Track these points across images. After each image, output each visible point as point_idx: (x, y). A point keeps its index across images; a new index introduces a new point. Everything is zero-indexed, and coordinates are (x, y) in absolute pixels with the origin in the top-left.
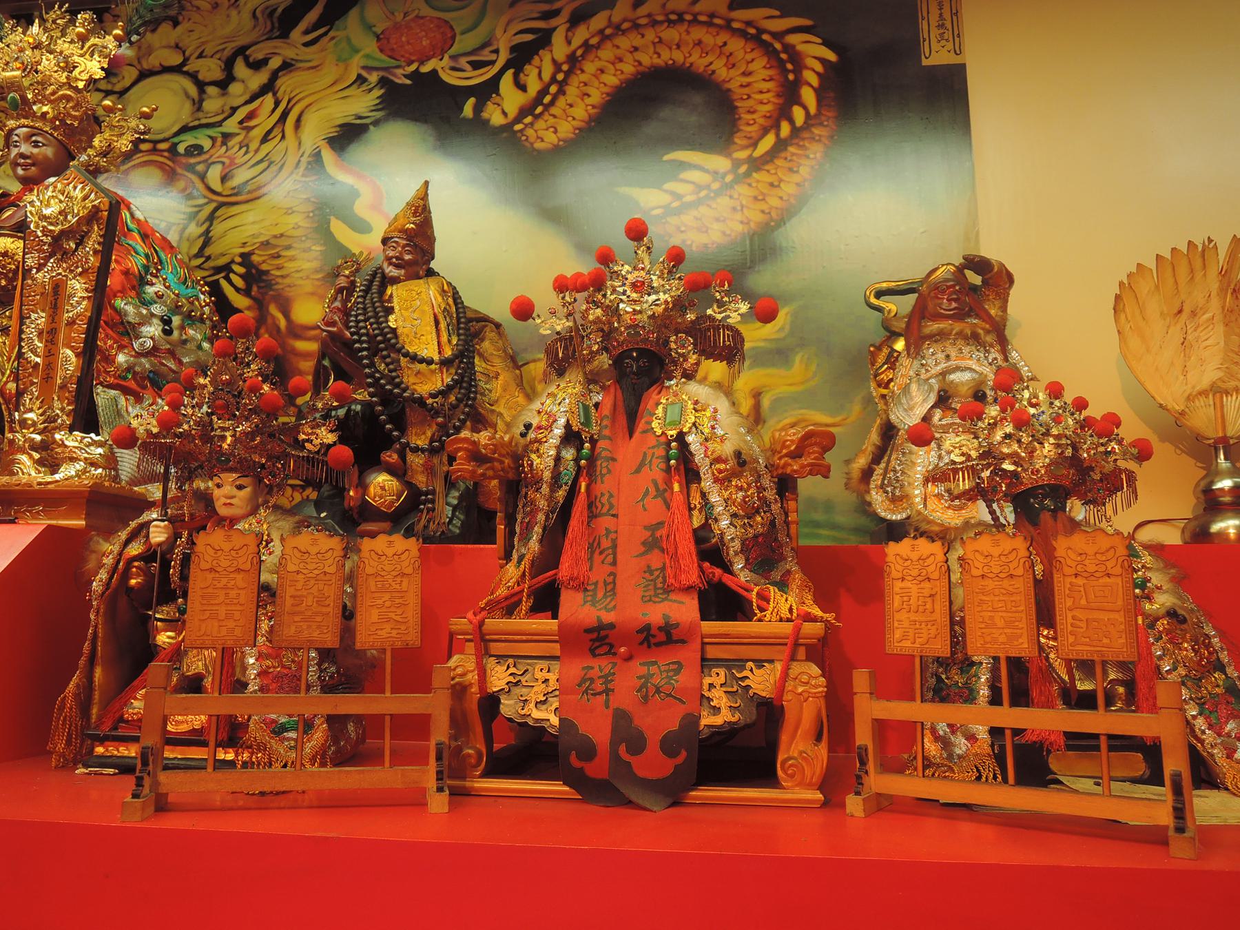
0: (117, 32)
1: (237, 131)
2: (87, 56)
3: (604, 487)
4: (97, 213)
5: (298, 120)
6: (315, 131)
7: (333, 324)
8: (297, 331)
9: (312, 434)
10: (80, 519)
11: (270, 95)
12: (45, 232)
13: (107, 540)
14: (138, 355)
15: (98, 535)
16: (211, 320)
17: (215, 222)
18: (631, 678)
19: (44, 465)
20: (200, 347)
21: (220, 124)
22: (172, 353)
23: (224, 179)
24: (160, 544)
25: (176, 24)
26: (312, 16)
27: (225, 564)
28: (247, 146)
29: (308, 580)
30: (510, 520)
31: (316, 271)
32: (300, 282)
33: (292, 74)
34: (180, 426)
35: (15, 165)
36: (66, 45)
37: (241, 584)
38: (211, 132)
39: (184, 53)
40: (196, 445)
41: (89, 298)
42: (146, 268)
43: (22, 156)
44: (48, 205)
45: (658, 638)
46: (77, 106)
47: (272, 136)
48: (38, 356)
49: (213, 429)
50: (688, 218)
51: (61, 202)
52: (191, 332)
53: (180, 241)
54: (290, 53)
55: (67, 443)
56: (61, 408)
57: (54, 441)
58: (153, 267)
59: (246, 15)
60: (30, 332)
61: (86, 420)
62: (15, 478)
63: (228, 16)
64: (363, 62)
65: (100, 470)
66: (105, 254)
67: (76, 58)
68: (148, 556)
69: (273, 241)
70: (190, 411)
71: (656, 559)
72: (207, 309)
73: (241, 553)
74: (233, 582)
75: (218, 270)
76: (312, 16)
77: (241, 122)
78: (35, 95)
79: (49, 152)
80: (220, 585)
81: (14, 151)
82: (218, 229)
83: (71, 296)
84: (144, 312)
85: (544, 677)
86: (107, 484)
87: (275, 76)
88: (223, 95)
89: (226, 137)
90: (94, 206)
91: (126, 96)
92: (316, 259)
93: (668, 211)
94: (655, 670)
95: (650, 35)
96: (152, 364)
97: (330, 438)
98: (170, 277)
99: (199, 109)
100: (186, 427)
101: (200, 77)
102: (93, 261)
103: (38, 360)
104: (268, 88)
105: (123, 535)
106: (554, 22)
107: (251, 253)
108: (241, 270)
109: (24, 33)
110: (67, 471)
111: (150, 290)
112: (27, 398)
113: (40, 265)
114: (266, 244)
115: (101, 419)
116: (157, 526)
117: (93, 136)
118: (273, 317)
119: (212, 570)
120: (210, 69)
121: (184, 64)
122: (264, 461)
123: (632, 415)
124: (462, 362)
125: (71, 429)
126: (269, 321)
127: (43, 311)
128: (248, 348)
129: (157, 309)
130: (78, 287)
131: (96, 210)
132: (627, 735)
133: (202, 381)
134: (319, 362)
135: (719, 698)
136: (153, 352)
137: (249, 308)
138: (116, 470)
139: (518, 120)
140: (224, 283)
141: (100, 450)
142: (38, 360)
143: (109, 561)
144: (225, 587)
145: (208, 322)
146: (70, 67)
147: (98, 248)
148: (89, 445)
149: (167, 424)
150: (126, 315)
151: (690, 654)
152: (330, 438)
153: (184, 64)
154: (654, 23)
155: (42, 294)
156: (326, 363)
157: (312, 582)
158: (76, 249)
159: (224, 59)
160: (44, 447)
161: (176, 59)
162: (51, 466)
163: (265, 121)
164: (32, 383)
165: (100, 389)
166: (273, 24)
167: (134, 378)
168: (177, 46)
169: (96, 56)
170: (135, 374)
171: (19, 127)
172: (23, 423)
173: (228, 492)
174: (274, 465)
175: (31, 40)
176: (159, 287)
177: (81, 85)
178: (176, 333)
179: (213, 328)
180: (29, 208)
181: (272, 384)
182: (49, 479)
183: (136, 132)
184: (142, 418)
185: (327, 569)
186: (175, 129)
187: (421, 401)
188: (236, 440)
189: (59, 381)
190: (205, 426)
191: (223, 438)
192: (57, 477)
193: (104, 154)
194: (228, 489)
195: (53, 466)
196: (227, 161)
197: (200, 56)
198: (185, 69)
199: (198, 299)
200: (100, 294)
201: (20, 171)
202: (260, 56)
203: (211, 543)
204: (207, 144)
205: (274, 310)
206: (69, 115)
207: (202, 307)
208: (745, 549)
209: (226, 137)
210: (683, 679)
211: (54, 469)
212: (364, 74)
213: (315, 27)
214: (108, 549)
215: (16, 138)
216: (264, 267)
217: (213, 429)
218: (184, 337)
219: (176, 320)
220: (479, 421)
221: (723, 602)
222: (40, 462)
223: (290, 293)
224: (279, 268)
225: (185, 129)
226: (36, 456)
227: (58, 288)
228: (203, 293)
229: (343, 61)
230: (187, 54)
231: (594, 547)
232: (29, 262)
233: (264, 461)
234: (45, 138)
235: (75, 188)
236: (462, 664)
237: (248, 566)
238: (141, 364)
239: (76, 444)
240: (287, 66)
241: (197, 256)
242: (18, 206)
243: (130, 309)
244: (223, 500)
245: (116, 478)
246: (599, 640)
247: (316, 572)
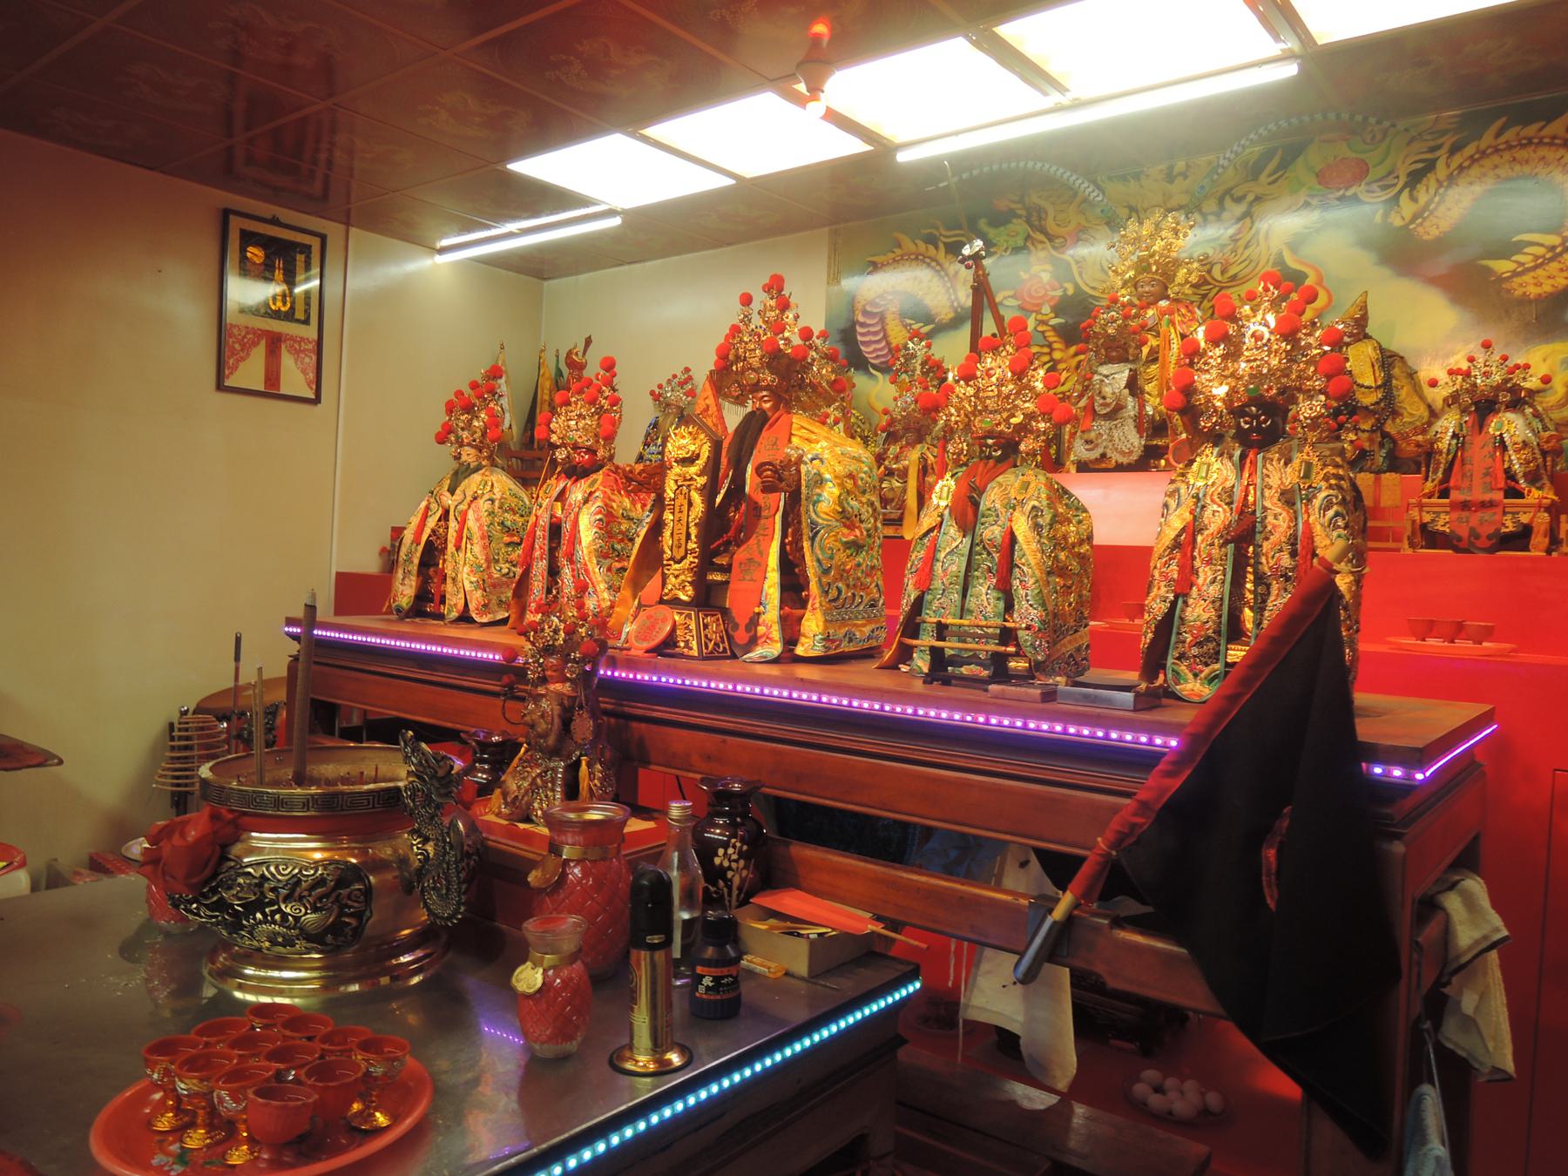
3: (1467, 454)
18: (1476, 519)
23: (1223, 272)
25: (1186, 177)
30: (1428, 467)
45: (1491, 504)
50: (1527, 278)
54: (1259, 190)
71: (1488, 479)
85: (1444, 518)
93: (1515, 274)
94: (1487, 515)
95: (1507, 156)
106: (1437, 154)
123: (1481, 425)
124: (1386, 385)
132: (1474, 534)
135: (1509, 523)
139: (1413, 220)
151: (1499, 510)
154: (1510, 147)
187: (1366, 408)
208: (1525, 475)
210: (1496, 517)
213: (1275, 172)
220: (1395, 413)
221: (1517, 494)
231: (1464, 475)
236: (1415, 513)
246: (1465, 506)
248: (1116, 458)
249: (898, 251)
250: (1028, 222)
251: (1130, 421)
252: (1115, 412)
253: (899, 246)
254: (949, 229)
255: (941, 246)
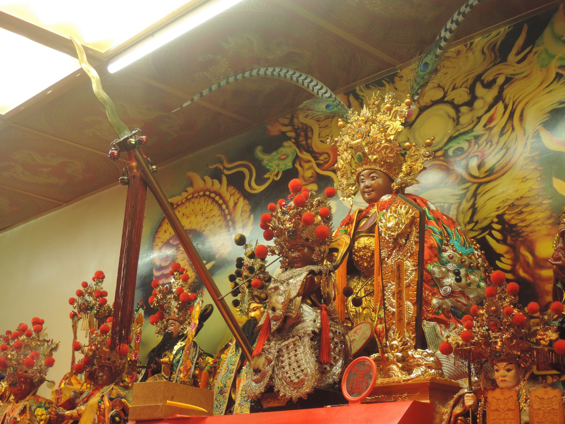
0: (408, 100)
1: (483, 132)
2: (393, 119)
4: (414, 220)
5: (521, 116)
6: (533, 119)
7: (559, 259)
8: (540, 263)
9: (544, 335)
10: (427, 399)
11: (501, 102)
12: (390, 236)
13: (443, 406)
14: (444, 297)
15: (439, 403)
16: (484, 266)
17: (478, 197)
19: (404, 371)
20: (479, 286)
21: (472, 130)
22: (462, 293)
24: (470, 406)
26: (520, 41)
27: (502, 406)
28: (491, 141)
29: (545, 413)
31: (549, 218)
32: (537, 228)
33: (514, 84)
34: (473, 338)
35: (363, 193)
36: (382, 116)
37: (511, 417)
38: (467, 137)
39: (444, 89)
40: (482, 348)
41: (416, 270)
42: (441, 241)
43: (367, 187)
44: (389, 221)
46: (392, 150)
47: (506, 130)
48: (394, 308)
49: (490, 339)
51: (395, 218)
52: (472, 277)
53: (457, 215)
54: (508, 71)
55: (415, 356)
56: (409, 336)
57: (408, 355)
58: (446, 238)
59: (478, 53)
60: (388, 294)
61: (421, 343)
62: (391, 379)
63: (467, 57)
64: (559, 63)
65: (433, 371)
66: (421, 242)
67: (387, 123)
68: (465, 414)
69: (516, 203)
70: (477, 329)
72: (480, 260)
73: (510, 400)
74: (507, 416)
75: (483, 230)
76: (520, 41)
77: (485, 126)
78: (370, 151)
79: (380, 181)
80: (502, 418)
81: (362, 185)
82: (480, 201)
83: (406, 270)
84: (444, 269)
86: (438, 378)
87: (502, 89)
88: (471, 110)
89: (477, 138)
90: (412, 217)
91: (414, 126)
92: (546, 210)
96: (452, 302)
97: (554, 336)
98: (456, 243)
99: (458, 123)
100: (476, 339)
101: (456, 102)
102: (416, 248)
103: (394, 310)
104: (499, 98)
105: (452, 402)
107: (503, 214)
108: (497, 227)
109: (359, 115)
110: (417, 372)
111: (445, 255)
112: (391, 332)
113: (389, 255)
114: (512, 206)
115: (428, 341)
116: (468, 396)
117: (402, 165)
118: (524, 256)
119: (496, 410)
120: (461, 96)
121: (445, 96)
122: (519, 353)
125: (416, 348)
126: (522, 259)
127: (393, 281)
128: (503, 290)
129: (451, 266)
130: (409, 264)
131: (414, 218)
133: (481, 312)
134: (555, 286)
136: (452, 294)
137: (507, 253)
138: (441, 370)
140: (489, 238)
141: (432, 359)
142: (394, 310)
143: (446, 417)
144: (504, 419)
145: (482, 268)
146: (384, 129)
147: (418, 240)
148: (426, 356)
149: (467, 338)
150: (434, 274)
152: (554, 336)
153: (445, 96)
155: (392, 271)
156: (559, 285)
157: (547, 414)
158: (406, 243)
159: (468, 86)
160: (403, 360)
161: (439, 95)
162: (408, 371)
163: (500, 121)
164: (393, 324)
165: (425, 322)
166: (495, 54)
167: (443, 312)
168: (439, 86)
169: (398, 118)
170: (443, 310)
171: (364, 170)
172: (392, 347)
173: (503, 373)
174: (525, 355)
175: (363, 118)
176: (450, 252)
177: (392, 137)
178: (463, 280)
179: (486, 271)
180: (380, 224)
181: (518, 308)
182: (408, 377)
183: (425, 157)
184: (453, 335)
185: (554, 407)
186: (445, 140)
188: (503, 343)
189: (406, 321)
190: (486, 337)
191: (496, 343)
192: (413, 376)
193: (408, 174)
194: (502, 372)
195: (408, 369)
196: (479, 154)
197: (454, 88)
198: (446, 99)
199: (474, 254)
200: (421, 265)
201: (366, 196)
202: (490, 78)
203: (493, 396)
204: (465, 145)
205: (524, 251)
206: (388, 157)
207: (477, 259)
209: (477, 138)
211: (410, 372)
212: (560, 71)
214: (445, 410)
215: (362, 177)
216: (513, 222)
217: (490, 339)
218: (469, 281)
219: (463, 271)
222: (402, 369)
223: (533, 237)
224: (523, 221)
225: (451, 139)
226: (400, 365)
227: (399, 267)
228: (476, 250)
229: (545, 66)
230: (446, 90)
232: (383, 255)
233: (519, 353)
234: (377, 174)
235: (401, 208)
237: (513, 407)
238: (446, 303)
239: (419, 356)
240: (509, 80)
241: (469, 223)
242: (368, 217)
243: (436, 269)
244: (501, 378)
245: (442, 375)
247: (549, 409)
248: (287, 392)
249: (190, 190)
250: (298, 144)
251: (307, 339)
252: (287, 325)
253: (191, 185)
254: (231, 161)
255: (224, 179)
